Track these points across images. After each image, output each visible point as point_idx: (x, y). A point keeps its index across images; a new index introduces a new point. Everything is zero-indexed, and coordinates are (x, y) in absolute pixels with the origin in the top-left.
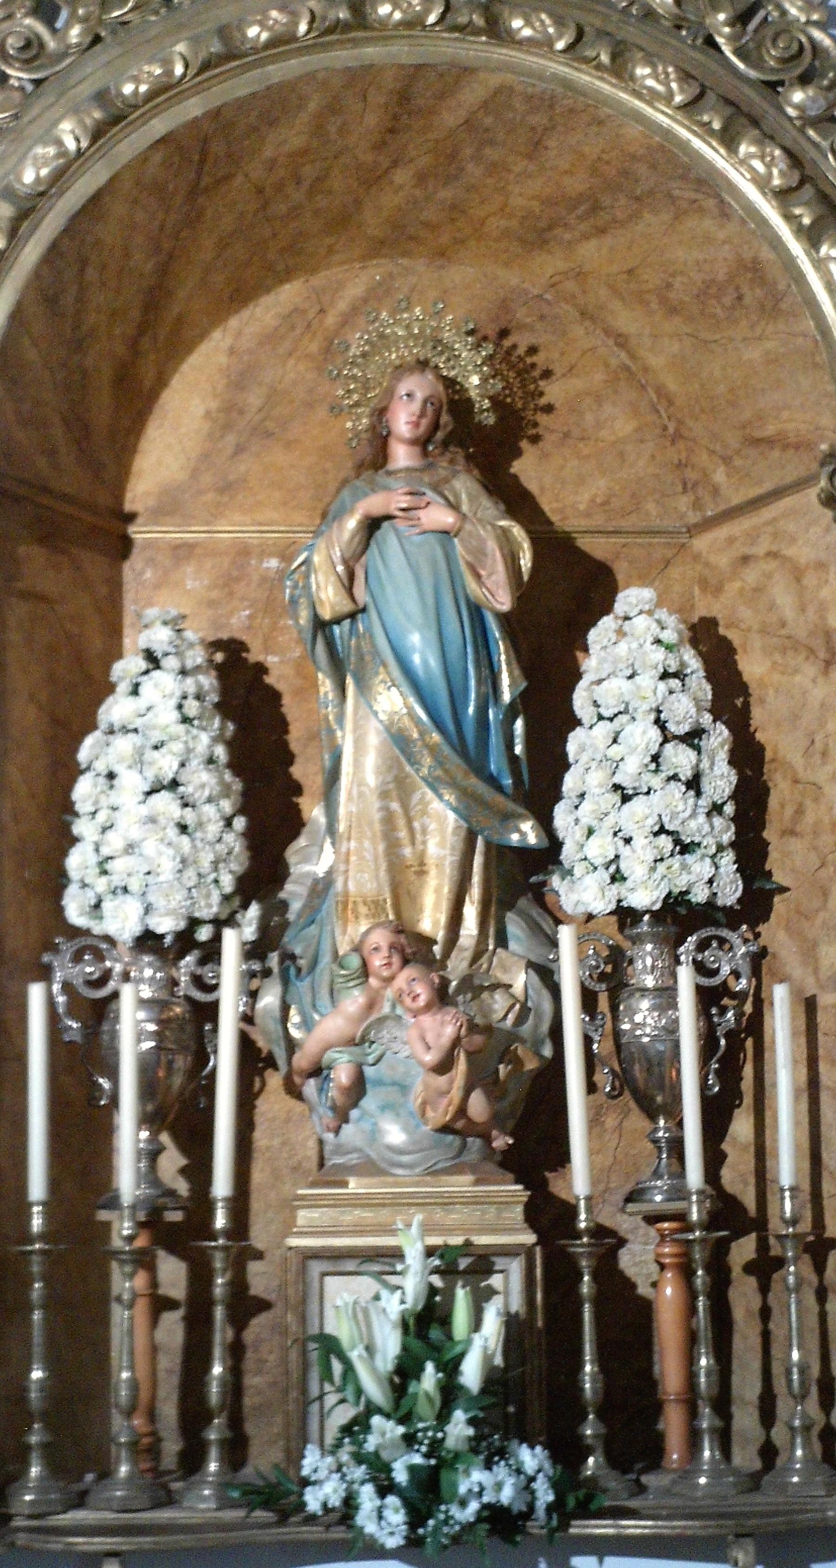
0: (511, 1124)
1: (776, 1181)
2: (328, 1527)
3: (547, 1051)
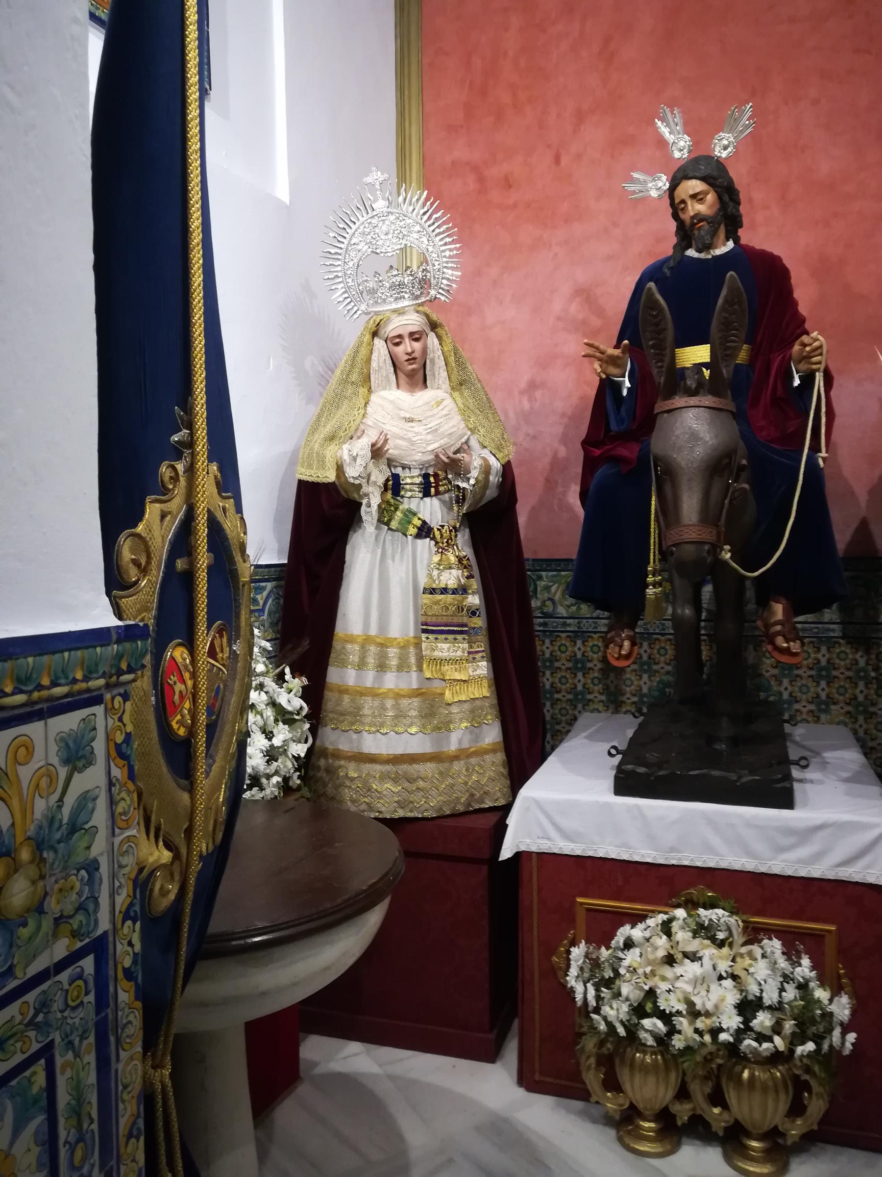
2: (134, 931)
3: (126, 552)
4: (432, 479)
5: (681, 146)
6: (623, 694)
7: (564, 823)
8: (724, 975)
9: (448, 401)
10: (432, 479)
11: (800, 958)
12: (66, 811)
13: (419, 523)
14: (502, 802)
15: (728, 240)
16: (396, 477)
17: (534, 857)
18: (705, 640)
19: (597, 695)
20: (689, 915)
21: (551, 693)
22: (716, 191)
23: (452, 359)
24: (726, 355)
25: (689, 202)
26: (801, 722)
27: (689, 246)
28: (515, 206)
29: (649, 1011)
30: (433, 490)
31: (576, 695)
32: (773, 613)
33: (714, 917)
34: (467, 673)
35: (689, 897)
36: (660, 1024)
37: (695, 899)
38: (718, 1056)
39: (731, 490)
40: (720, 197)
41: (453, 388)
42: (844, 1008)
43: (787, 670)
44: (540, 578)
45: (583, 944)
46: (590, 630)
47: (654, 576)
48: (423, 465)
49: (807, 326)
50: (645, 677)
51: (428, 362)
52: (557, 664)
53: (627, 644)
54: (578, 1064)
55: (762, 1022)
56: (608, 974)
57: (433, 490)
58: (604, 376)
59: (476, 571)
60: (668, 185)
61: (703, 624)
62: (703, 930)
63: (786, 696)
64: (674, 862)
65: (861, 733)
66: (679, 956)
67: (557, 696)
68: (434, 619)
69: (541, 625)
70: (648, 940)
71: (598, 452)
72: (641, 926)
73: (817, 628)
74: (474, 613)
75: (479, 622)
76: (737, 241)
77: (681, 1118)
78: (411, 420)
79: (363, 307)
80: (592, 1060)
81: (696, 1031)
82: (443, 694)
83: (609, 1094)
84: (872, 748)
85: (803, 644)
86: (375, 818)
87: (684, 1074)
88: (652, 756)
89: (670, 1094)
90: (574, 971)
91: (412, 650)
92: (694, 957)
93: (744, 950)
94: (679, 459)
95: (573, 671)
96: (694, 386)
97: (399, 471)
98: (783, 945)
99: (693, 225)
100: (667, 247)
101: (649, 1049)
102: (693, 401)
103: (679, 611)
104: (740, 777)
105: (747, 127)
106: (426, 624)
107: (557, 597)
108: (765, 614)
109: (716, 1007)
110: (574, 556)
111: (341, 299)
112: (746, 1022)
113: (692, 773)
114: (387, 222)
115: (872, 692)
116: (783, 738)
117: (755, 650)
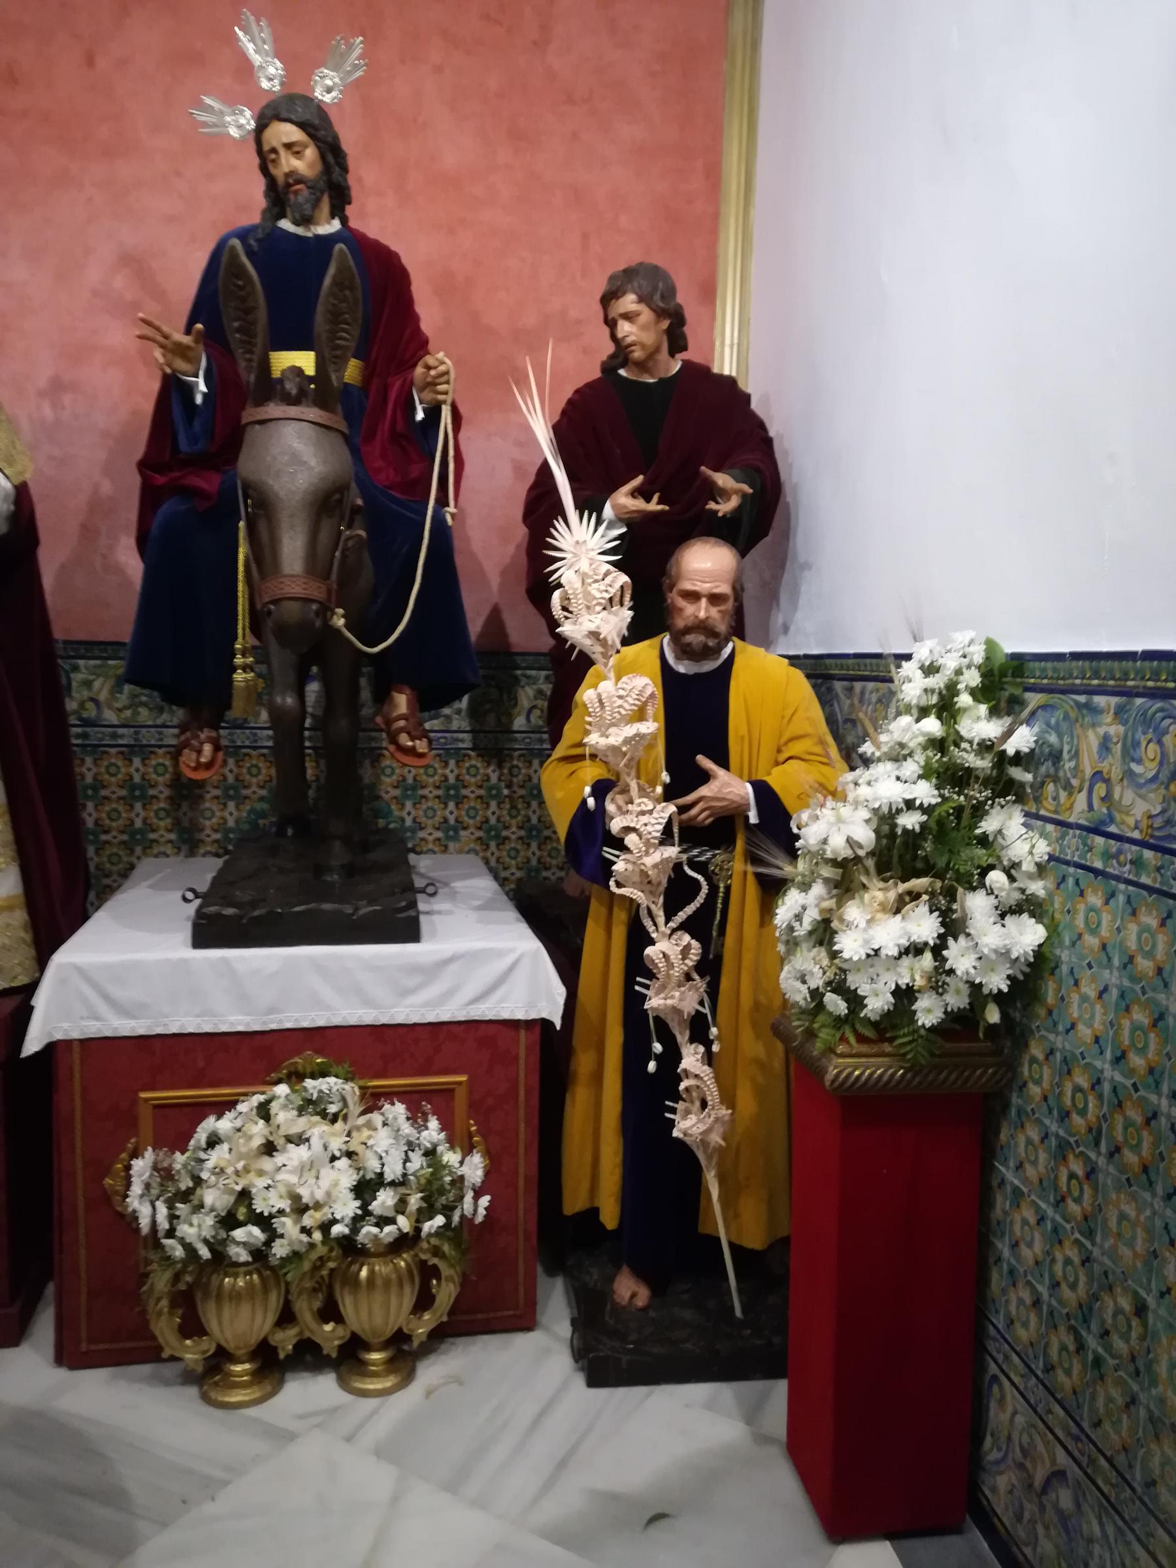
0: (73, 1096)
5: (271, 76)
6: (202, 830)
8: (337, 1154)
11: (426, 1120)
14: (22, 980)
15: (333, 218)
17: (76, 1048)
18: (309, 755)
19: (164, 833)
20: (293, 1091)
21: (95, 834)
22: (319, 148)
24: (336, 357)
25: (283, 152)
26: (426, 853)
27: (282, 215)
29: (241, 1218)
32: (395, 706)
33: (324, 1088)
35: (292, 1069)
36: (256, 1231)
37: (300, 1068)
38: (329, 1259)
39: (343, 538)
40: (323, 157)
42: (477, 1168)
43: (411, 790)
44: (76, 669)
45: (149, 1154)
46: (153, 742)
47: (244, 656)
49: (431, 347)
50: (231, 805)
52: (103, 793)
53: (207, 748)
54: (144, 1312)
55: (384, 1203)
56: (186, 1183)
58: (168, 371)
61: (307, 733)
62: (312, 1106)
64: (274, 1026)
65: (493, 863)
66: (280, 1142)
67: (104, 837)
69: (78, 736)
70: (239, 1130)
71: (161, 480)
72: (229, 1115)
73: (445, 738)
76: (344, 221)
77: (283, 1349)
80: (164, 1303)
81: (304, 1230)
83: (188, 1342)
84: (505, 879)
87: (287, 1292)
89: (271, 1318)
90: (136, 1189)
92: (299, 1140)
93: (362, 1120)
94: (276, 488)
95: (129, 802)
96: (294, 392)
98: (408, 1109)
99: (288, 185)
101: (242, 1269)
102: (293, 411)
103: (279, 700)
104: (357, 909)
105: (356, 67)
107: (103, 696)
108: (386, 707)
109: (328, 1194)
110: (127, 639)
112: (364, 1207)
113: (297, 909)
115: (505, 812)
116: (409, 869)
117: (373, 766)
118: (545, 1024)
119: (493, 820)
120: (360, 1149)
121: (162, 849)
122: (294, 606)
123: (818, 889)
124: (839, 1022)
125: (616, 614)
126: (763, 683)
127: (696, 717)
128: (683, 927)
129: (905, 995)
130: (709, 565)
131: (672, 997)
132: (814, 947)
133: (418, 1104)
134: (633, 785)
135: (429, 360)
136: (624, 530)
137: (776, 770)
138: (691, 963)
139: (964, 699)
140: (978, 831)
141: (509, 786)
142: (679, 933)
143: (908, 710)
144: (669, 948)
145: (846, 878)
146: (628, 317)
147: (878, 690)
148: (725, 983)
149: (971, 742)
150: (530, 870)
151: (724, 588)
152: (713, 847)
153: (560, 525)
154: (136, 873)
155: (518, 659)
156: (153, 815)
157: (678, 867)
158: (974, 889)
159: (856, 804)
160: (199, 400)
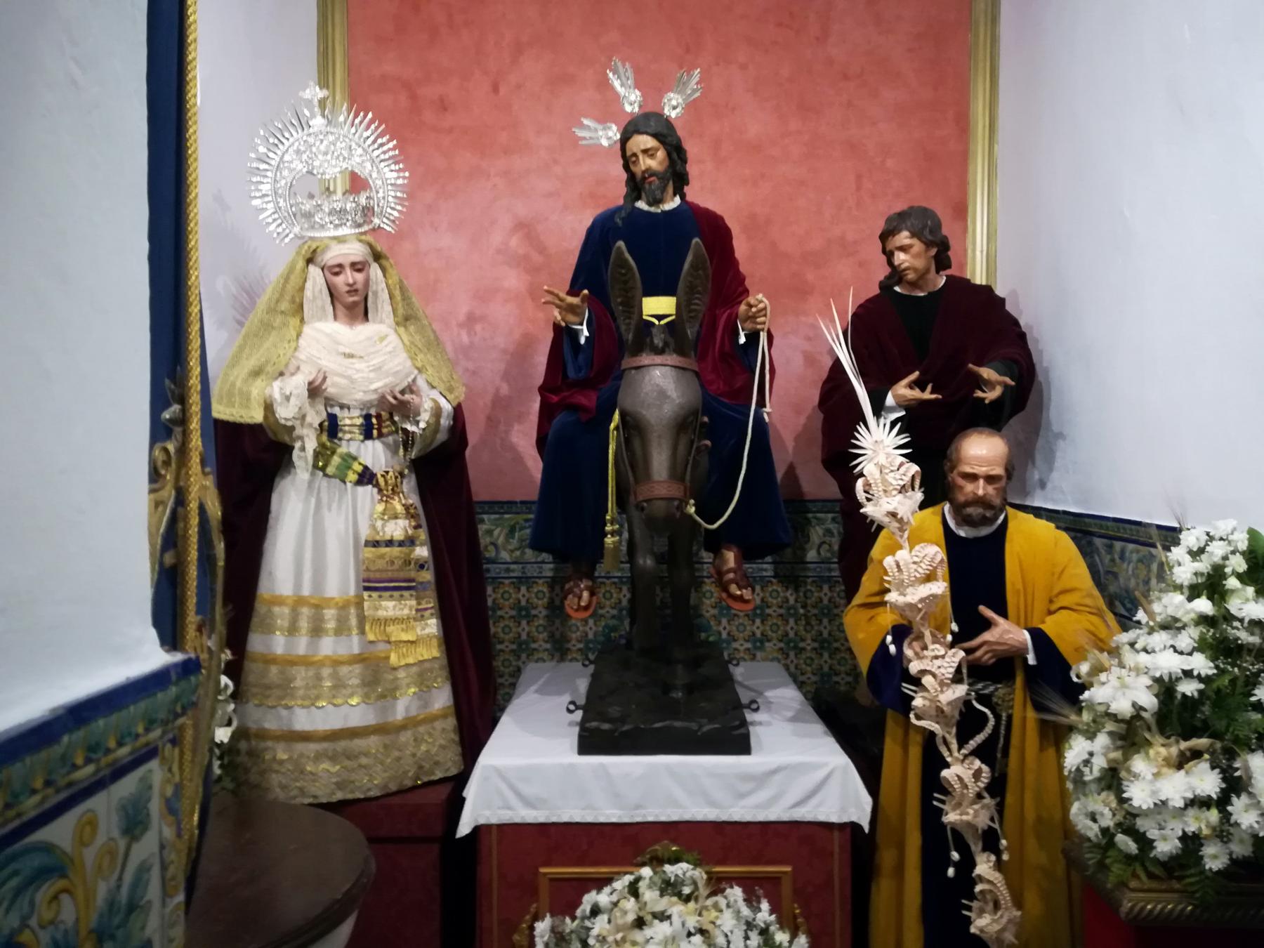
0: (492, 868)
1: (131, 753)
4: (374, 421)
5: (632, 101)
6: (569, 641)
7: (527, 790)
8: (693, 931)
9: (393, 337)
10: (374, 421)
11: (759, 902)
12: (125, 891)
13: (359, 468)
14: (454, 771)
15: (675, 195)
16: (332, 419)
17: (494, 831)
19: (542, 644)
20: (655, 873)
23: (397, 293)
25: (641, 157)
27: (639, 198)
28: (450, 131)
30: (375, 432)
31: (520, 645)
32: (725, 561)
33: (680, 873)
34: (414, 631)
37: (660, 854)
40: (669, 155)
41: (397, 324)
44: (482, 521)
48: (365, 405)
51: (370, 294)
53: (586, 594)
57: (375, 432)
59: (423, 521)
60: (618, 136)
62: (669, 887)
63: (724, 635)
64: (639, 819)
65: (792, 669)
66: (648, 918)
68: (378, 575)
71: (555, 399)
72: (607, 890)
74: (422, 567)
75: (428, 576)
76: (683, 197)
78: (351, 356)
79: (297, 229)
82: (388, 658)
85: (753, 590)
86: (310, 805)
88: (614, 711)
91: (353, 611)
92: (663, 917)
93: (709, 902)
95: (517, 620)
96: (661, 345)
97: (336, 410)
98: (744, 892)
99: (644, 179)
100: (615, 192)
102: (658, 359)
104: (701, 727)
106: (368, 581)
107: (501, 541)
111: (270, 220)
114: (325, 142)
116: (730, 679)
118: (854, 827)
119: (792, 634)
120: (709, 927)
121: (540, 655)
122: (662, 504)
123: (1102, 740)
124: (1129, 859)
125: (910, 498)
126: (1032, 545)
127: (977, 573)
128: (976, 753)
129: (1191, 842)
130: (984, 452)
131: (967, 814)
132: (1103, 790)
133: (753, 888)
134: (927, 634)
135: (751, 300)
136: (903, 413)
137: (1049, 619)
138: (982, 785)
139: (1232, 583)
140: (1253, 699)
141: (804, 607)
142: (971, 758)
143: (1179, 588)
144: (961, 771)
145: (1130, 734)
146: (903, 249)
147: (1138, 552)
148: (1010, 799)
149: (1241, 620)
150: (822, 675)
151: (999, 471)
152: (995, 681)
153: (862, 429)
154: (523, 678)
155: (810, 505)
156: (536, 630)
157: (967, 703)
158: (1253, 751)
159: (1138, 671)
160: (583, 341)
